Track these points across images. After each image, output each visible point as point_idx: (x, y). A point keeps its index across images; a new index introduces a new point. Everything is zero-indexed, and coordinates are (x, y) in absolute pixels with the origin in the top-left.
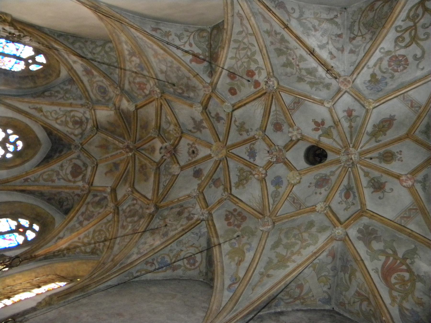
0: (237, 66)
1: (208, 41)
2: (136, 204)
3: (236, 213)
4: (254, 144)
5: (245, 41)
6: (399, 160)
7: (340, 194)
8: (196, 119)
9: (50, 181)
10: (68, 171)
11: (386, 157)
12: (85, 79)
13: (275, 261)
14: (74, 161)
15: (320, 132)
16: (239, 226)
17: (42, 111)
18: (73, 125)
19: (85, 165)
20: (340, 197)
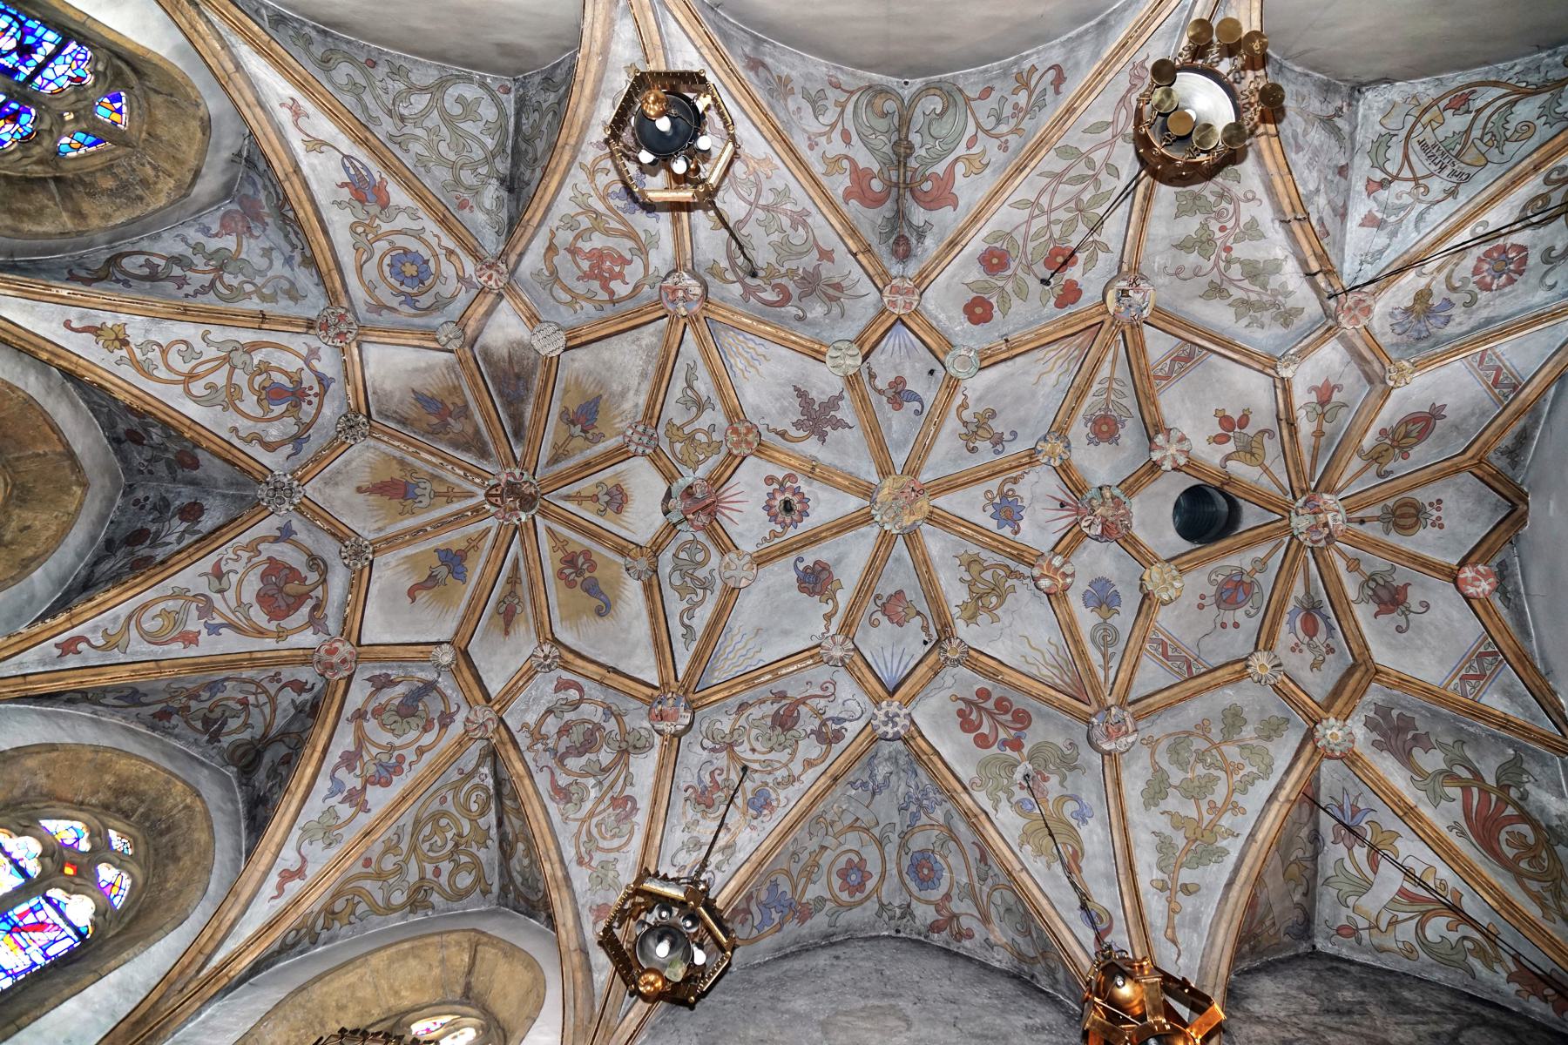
0: (1027, 233)
1: (899, 131)
2: (581, 700)
3: (990, 704)
4: (1015, 481)
5: (1099, 156)
6: (1433, 525)
7: (1291, 622)
8: (813, 394)
9: (174, 640)
10: (249, 595)
11: (1403, 516)
12: (340, 222)
13: (1180, 841)
14: (268, 550)
15: (1230, 447)
16: (1016, 745)
17: (124, 343)
18: (259, 401)
19: (315, 561)
20: (1293, 631)
